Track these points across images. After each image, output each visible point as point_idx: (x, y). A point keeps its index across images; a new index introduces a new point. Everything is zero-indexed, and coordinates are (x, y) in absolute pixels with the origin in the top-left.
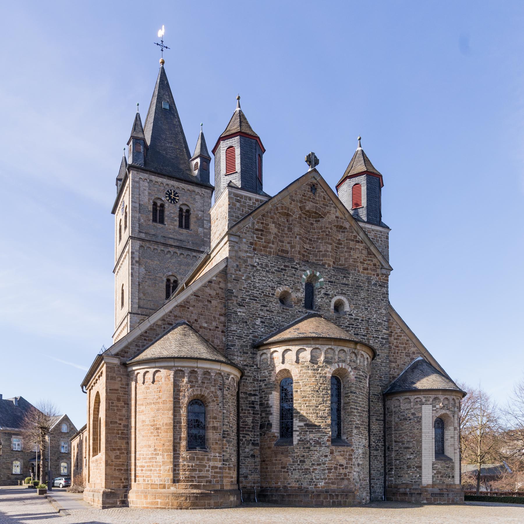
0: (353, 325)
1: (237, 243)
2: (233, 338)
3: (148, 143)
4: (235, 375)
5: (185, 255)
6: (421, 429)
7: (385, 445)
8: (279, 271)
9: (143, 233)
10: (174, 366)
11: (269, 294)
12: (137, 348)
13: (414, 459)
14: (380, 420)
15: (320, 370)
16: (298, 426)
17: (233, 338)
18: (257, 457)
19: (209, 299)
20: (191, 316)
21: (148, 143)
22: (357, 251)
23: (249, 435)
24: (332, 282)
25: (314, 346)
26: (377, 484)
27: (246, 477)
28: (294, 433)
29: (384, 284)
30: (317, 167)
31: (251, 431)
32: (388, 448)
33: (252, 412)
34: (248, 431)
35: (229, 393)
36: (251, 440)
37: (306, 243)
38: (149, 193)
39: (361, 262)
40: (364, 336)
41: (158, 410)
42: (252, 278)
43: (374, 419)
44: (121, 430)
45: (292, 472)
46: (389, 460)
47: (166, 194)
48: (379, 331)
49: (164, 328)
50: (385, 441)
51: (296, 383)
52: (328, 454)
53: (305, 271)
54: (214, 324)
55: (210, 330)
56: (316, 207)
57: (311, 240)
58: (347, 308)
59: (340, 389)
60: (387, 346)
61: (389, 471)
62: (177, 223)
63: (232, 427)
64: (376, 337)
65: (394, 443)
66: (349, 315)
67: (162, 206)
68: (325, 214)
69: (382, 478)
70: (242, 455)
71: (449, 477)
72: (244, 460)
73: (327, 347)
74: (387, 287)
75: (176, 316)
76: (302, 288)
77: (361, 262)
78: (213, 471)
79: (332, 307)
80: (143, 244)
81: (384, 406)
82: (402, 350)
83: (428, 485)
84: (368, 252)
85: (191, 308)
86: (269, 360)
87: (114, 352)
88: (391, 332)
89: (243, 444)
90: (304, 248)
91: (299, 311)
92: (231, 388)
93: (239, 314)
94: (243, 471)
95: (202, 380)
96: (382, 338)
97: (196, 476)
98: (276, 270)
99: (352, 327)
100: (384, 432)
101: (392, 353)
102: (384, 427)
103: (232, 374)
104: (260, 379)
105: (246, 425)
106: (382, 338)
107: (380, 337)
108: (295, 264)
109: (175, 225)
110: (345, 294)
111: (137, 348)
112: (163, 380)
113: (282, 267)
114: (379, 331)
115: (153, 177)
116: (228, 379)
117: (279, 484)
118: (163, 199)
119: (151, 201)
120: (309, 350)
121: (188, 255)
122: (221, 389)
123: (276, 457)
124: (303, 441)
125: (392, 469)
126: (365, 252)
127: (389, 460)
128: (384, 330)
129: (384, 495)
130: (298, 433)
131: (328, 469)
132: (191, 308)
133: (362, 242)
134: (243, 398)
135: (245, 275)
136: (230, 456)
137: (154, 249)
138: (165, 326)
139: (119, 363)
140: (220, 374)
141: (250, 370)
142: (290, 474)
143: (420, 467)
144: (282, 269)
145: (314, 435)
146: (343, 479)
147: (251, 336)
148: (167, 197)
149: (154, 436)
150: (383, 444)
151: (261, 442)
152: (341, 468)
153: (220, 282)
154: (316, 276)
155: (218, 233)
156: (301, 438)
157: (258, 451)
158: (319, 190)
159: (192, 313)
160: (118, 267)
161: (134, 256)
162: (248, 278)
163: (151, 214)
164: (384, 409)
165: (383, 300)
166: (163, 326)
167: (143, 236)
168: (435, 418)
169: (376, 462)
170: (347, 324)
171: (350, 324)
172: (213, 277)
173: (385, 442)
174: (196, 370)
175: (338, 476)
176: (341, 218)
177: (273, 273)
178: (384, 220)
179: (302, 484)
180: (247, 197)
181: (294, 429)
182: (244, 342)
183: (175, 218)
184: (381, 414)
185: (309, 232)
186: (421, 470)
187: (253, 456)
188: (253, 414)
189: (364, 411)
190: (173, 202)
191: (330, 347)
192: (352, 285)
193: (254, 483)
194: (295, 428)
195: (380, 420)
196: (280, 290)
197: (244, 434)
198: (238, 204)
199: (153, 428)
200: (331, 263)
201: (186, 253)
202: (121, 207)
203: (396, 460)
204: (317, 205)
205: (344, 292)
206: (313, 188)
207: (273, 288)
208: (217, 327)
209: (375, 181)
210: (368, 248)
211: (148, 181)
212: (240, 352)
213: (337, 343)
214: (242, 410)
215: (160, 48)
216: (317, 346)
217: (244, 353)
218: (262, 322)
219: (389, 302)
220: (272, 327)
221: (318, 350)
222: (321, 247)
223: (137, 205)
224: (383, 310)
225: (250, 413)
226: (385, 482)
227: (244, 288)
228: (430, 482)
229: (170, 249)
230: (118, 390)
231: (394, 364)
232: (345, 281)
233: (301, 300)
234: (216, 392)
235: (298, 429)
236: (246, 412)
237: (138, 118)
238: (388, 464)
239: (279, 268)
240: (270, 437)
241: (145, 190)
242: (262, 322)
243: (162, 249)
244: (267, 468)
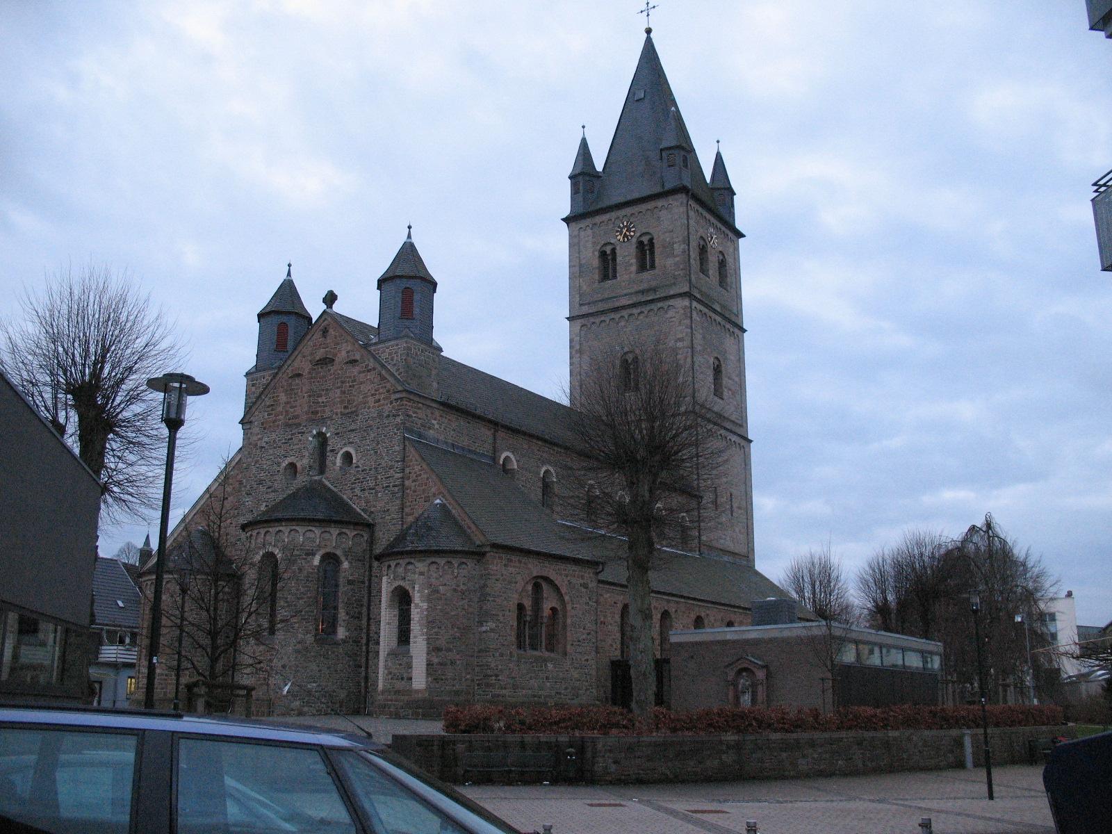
3: (599, 166)
5: (646, 312)
21: (599, 166)
38: (594, 243)
39: (372, 395)
47: (617, 231)
57: (327, 390)
60: (400, 494)
62: (634, 268)
67: (614, 250)
71: (402, 679)
96: (394, 486)
107: (391, 484)
110: (350, 443)
113: (290, 437)
121: (631, 315)
133: (374, 369)
161: (573, 344)
162: (257, 462)
170: (353, 481)
177: (280, 447)
198: (253, 389)
201: (646, 309)
210: (380, 374)
215: (644, 7)
223: (577, 269)
229: (625, 313)
232: (353, 427)
237: (584, 145)
241: (587, 241)
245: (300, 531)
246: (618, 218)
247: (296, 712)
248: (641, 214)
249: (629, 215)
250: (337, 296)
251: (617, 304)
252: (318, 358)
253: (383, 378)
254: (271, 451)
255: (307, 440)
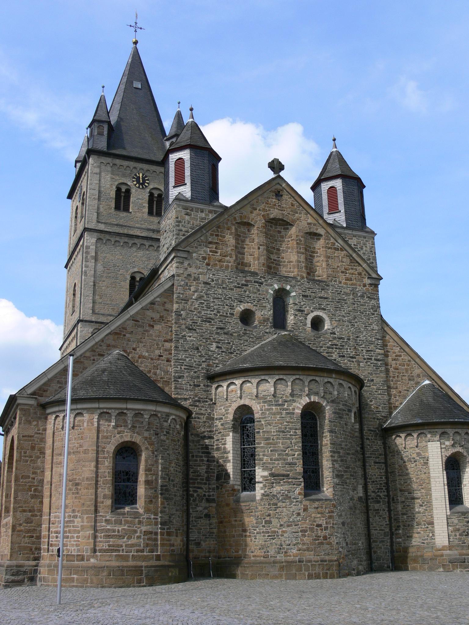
0: (336, 345)
1: (186, 258)
2: (181, 368)
4: (176, 415)
6: (429, 473)
7: (388, 496)
8: (239, 287)
9: (102, 223)
10: (99, 408)
11: (227, 314)
12: (59, 385)
13: (424, 513)
14: (380, 463)
15: (286, 405)
16: (262, 477)
17: (181, 368)
18: (214, 517)
19: (152, 323)
20: (127, 344)
22: (336, 259)
23: (202, 488)
24: (307, 296)
25: (277, 377)
26: (381, 548)
27: (198, 544)
28: (257, 485)
29: (374, 295)
30: (282, 174)
31: (205, 484)
32: (393, 499)
33: (206, 459)
34: (201, 483)
35: (168, 439)
36: (205, 495)
37: (273, 254)
40: (352, 358)
41: (78, 461)
42: (205, 296)
43: (370, 462)
44: (34, 486)
45: (255, 536)
46: (395, 515)
47: (134, 178)
48: (372, 351)
49: (94, 360)
50: (388, 491)
51: (258, 421)
52: (301, 511)
53: (272, 285)
54: (157, 352)
55: (152, 359)
56: (283, 214)
58: (327, 326)
59: (317, 428)
60: (383, 369)
61: (396, 530)
62: (146, 210)
63: (173, 481)
64: (368, 359)
65: (399, 494)
66: (331, 333)
67: (128, 192)
68: (294, 221)
69: (387, 539)
70: (193, 514)
72: (195, 521)
73: (294, 377)
74: (378, 299)
75: (109, 346)
76: (269, 306)
77: (342, 272)
78: (146, 537)
79: (309, 325)
80: (102, 236)
81: (384, 443)
82: (403, 373)
83: (444, 547)
84: (351, 260)
85: (128, 335)
86: (225, 393)
87: (30, 391)
88: (387, 351)
89: (194, 501)
90: (271, 259)
91: (266, 333)
92: (171, 432)
93: (188, 338)
94: (193, 536)
95: (133, 423)
97: (124, 545)
98: (235, 287)
99: (336, 348)
100: (387, 478)
101: (390, 377)
102: (387, 472)
103: (172, 414)
104: (215, 417)
105: (198, 476)
106: (376, 360)
107: (373, 358)
108: (259, 277)
109: (143, 213)
111: (59, 385)
112: (85, 424)
113: (243, 282)
114: (372, 351)
115: (118, 160)
116: (167, 422)
117: (240, 553)
118: (129, 183)
119: (114, 187)
120: (272, 381)
122: (157, 434)
123: (236, 517)
124: (268, 495)
125: (399, 526)
126: (347, 260)
127: (395, 515)
128: (377, 350)
129: (392, 563)
130: (261, 485)
131: (301, 531)
132: (128, 335)
133: (342, 250)
134: (193, 441)
135: (196, 294)
136: (170, 517)
137: (116, 241)
138: (95, 358)
139: (36, 404)
140: (156, 415)
141: (202, 407)
142: (253, 538)
143: (432, 523)
144: (243, 285)
145: (282, 488)
146: (322, 543)
147: (204, 365)
148: (134, 181)
149: (73, 493)
150: (386, 493)
151: (218, 497)
152: (319, 528)
153: (165, 303)
154: (286, 290)
155: (166, 246)
156: (265, 492)
157: (214, 510)
158: (285, 197)
159: (129, 340)
160: (71, 262)
163: (114, 201)
164: (385, 448)
165: (373, 314)
166: (92, 358)
167: (102, 227)
168: (444, 459)
169: (377, 518)
171: (332, 345)
172: (157, 297)
173: (388, 491)
174: (125, 411)
175: (315, 540)
176: (315, 225)
178: (369, 224)
179: (268, 552)
180: (198, 208)
181: (257, 480)
182: (195, 372)
183: (144, 205)
184: (380, 455)
185: (276, 241)
186: (433, 527)
187: (208, 516)
188: (208, 461)
189: (348, 454)
190: (141, 187)
191: (298, 377)
192: (333, 299)
193: (209, 552)
194: (258, 478)
195: (380, 463)
196: (241, 308)
197: (195, 487)
199: (71, 483)
200: (305, 275)
202: (79, 192)
203: (403, 514)
204: (284, 212)
205: (323, 306)
206: (278, 194)
207: (232, 307)
208: (160, 356)
209: (354, 184)
211: (111, 165)
212: (190, 385)
213: (307, 373)
214: (193, 456)
216: (281, 377)
217: (195, 385)
218: (217, 347)
219: (381, 316)
220: (231, 353)
221: (283, 382)
222: (292, 257)
224: (375, 327)
225: (203, 460)
226: (392, 545)
227: (195, 309)
228: (446, 543)
229: (136, 241)
230: (33, 436)
231: (394, 390)
232: (323, 294)
233: (268, 319)
234: (150, 438)
235: (261, 480)
236: (198, 459)
238: (395, 520)
239: (238, 284)
240: (228, 490)
242: (217, 347)
243: (126, 241)
244: (225, 532)
245: (345, 386)
246: (135, 168)
247: (356, 572)
248: (155, 173)
249: (145, 169)
250: (284, 166)
251: (131, 232)
252: (272, 216)
253: (353, 261)
254: (220, 291)
255: (267, 291)
